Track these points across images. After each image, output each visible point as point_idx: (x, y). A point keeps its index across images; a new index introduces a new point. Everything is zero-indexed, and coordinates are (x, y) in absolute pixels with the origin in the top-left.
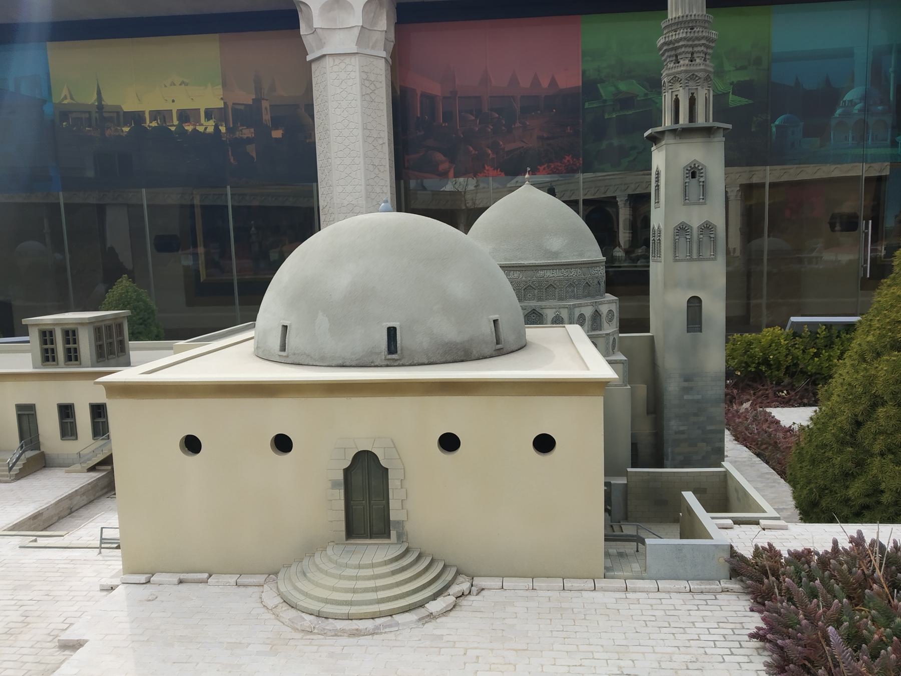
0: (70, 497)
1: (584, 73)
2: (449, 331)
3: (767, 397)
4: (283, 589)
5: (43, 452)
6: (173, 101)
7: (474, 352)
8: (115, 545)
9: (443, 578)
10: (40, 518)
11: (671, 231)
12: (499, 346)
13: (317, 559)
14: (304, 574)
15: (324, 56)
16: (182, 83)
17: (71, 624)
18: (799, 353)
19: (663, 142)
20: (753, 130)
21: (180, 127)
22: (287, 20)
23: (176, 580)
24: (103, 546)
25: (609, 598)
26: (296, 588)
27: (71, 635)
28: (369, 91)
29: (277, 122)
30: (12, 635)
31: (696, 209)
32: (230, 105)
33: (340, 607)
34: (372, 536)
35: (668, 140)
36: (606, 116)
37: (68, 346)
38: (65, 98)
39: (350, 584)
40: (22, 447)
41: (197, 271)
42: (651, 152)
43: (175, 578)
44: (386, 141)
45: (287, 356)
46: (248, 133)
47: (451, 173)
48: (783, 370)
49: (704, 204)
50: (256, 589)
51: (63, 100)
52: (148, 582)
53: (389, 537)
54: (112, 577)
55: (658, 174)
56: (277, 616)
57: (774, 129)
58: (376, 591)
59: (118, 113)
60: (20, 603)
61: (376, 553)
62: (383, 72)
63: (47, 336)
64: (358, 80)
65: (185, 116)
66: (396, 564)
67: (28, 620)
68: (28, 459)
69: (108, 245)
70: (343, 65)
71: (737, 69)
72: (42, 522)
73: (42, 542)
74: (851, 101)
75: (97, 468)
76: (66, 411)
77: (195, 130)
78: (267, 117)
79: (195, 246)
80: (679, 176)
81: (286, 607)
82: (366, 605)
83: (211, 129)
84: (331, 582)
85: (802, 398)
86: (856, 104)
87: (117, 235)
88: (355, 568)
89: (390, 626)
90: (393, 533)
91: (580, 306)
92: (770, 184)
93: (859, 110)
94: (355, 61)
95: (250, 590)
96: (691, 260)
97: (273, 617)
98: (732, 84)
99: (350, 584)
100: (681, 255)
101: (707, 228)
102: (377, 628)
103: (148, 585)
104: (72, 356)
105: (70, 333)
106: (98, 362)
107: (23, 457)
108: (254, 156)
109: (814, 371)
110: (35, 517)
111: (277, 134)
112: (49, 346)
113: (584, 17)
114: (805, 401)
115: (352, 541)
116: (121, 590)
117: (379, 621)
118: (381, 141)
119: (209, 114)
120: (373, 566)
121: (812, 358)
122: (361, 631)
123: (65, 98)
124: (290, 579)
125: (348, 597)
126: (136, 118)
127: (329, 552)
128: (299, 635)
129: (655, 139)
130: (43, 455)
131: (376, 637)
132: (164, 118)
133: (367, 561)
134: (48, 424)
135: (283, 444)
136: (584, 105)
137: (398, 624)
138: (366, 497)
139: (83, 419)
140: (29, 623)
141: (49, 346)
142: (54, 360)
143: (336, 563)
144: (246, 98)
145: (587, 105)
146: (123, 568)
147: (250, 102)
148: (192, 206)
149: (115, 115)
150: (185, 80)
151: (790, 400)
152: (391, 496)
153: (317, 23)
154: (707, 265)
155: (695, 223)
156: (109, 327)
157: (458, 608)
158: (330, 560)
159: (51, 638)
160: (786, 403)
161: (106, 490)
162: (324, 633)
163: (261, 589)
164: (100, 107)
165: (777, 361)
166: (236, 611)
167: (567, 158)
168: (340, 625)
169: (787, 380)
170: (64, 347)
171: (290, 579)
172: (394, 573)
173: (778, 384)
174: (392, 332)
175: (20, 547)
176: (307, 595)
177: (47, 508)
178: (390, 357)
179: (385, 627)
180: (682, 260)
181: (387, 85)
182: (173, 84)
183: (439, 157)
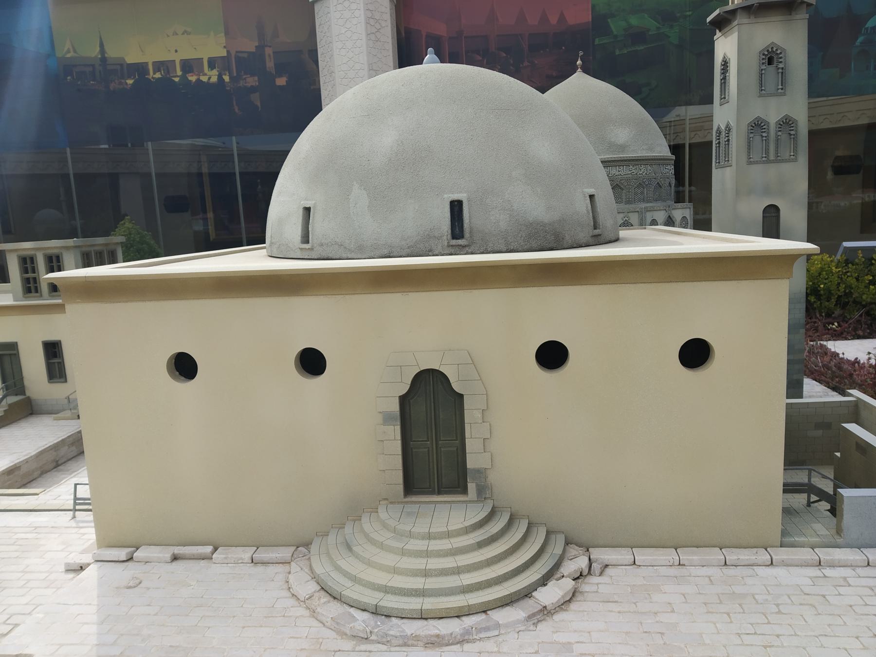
0: (56, 447)
1: (593, 7)
2: (535, 207)
3: (816, 330)
4: (319, 570)
5: (29, 398)
6: (176, 51)
7: (567, 237)
9: (554, 548)
10: (16, 473)
11: (744, 128)
12: (597, 232)
13: (367, 524)
14: (349, 548)
16: (185, 32)
17: (16, 625)
18: (853, 281)
19: (736, 23)
21: (184, 77)
23: (168, 556)
24: (78, 507)
25: (802, 577)
26: (338, 569)
28: (374, 30)
29: (281, 69)
31: (773, 102)
32: (233, 54)
33: (405, 599)
35: (740, 19)
36: (617, 52)
38: (68, 52)
39: (419, 564)
41: (207, 233)
42: (714, 42)
43: (166, 553)
45: (312, 249)
46: (252, 81)
48: (833, 300)
49: (784, 94)
50: (280, 568)
52: (130, 559)
53: (464, 491)
54: (83, 552)
55: (725, 64)
56: (313, 613)
58: (459, 573)
59: (121, 65)
61: (451, 515)
62: (388, 10)
63: (27, 263)
64: (362, 19)
65: (188, 66)
66: (481, 531)
68: (10, 405)
77: (198, 80)
78: (270, 64)
79: (205, 211)
80: (754, 62)
81: (325, 598)
83: (214, 79)
84: (390, 560)
85: (855, 329)
88: (423, 538)
89: (487, 629)
90: (471, 487)
91: (652, 210)
95: (272, 569)
96: (769, 161)
99: (419, 564)
100: (756, 157)
101: (787, 123)
102: (467, 632)
103: (130, 564)
108: (259, 104)
109: (869, 300)
111: (281, 81)
114: (860, 333)
115: (414, 498)
116: (92, 571)
117: (469, 621)
119: (212, 63)
120: (449, 535)
121: (867, 287)
122: (443, 637)
123: (68, 52)
124: (328, 554)
125: (418, 583)
126: (140, 69)
127: (383, 514)
128: (348, 645)
129: (722, 23)
131: (467, 647)
133: (439, 527)
135: (312, 362)
136: (594, 41)
137: (498, 626)
138: (432, 435)
142: (37, 292)
143: (395, 531)
144: (249, 45)
145: (597, 41)
146: (98, 540)
147: (254, 50)
148: (200, 175)
149: (118, 67)
150: (189, 30)
151: (842, 333)
152: (467, 435)
154: (786, 167)
155: (773, 118)
157: (579, 597)
158: (385, 526)
160: (839, 336)
162: (385, 640)
163: (286, 568)
164: (104, 60)
165: (829, 292)
169: (838, 312)
171: (328, 554)
172: (481, 545)
173: (829, 315)
174: (456, 209)
176: (355, 579)
177: (26, 461)
178: (454, 242)
179: (480, 630)
180: (756, 163)
181: (392, 24)
182: (175, 34)
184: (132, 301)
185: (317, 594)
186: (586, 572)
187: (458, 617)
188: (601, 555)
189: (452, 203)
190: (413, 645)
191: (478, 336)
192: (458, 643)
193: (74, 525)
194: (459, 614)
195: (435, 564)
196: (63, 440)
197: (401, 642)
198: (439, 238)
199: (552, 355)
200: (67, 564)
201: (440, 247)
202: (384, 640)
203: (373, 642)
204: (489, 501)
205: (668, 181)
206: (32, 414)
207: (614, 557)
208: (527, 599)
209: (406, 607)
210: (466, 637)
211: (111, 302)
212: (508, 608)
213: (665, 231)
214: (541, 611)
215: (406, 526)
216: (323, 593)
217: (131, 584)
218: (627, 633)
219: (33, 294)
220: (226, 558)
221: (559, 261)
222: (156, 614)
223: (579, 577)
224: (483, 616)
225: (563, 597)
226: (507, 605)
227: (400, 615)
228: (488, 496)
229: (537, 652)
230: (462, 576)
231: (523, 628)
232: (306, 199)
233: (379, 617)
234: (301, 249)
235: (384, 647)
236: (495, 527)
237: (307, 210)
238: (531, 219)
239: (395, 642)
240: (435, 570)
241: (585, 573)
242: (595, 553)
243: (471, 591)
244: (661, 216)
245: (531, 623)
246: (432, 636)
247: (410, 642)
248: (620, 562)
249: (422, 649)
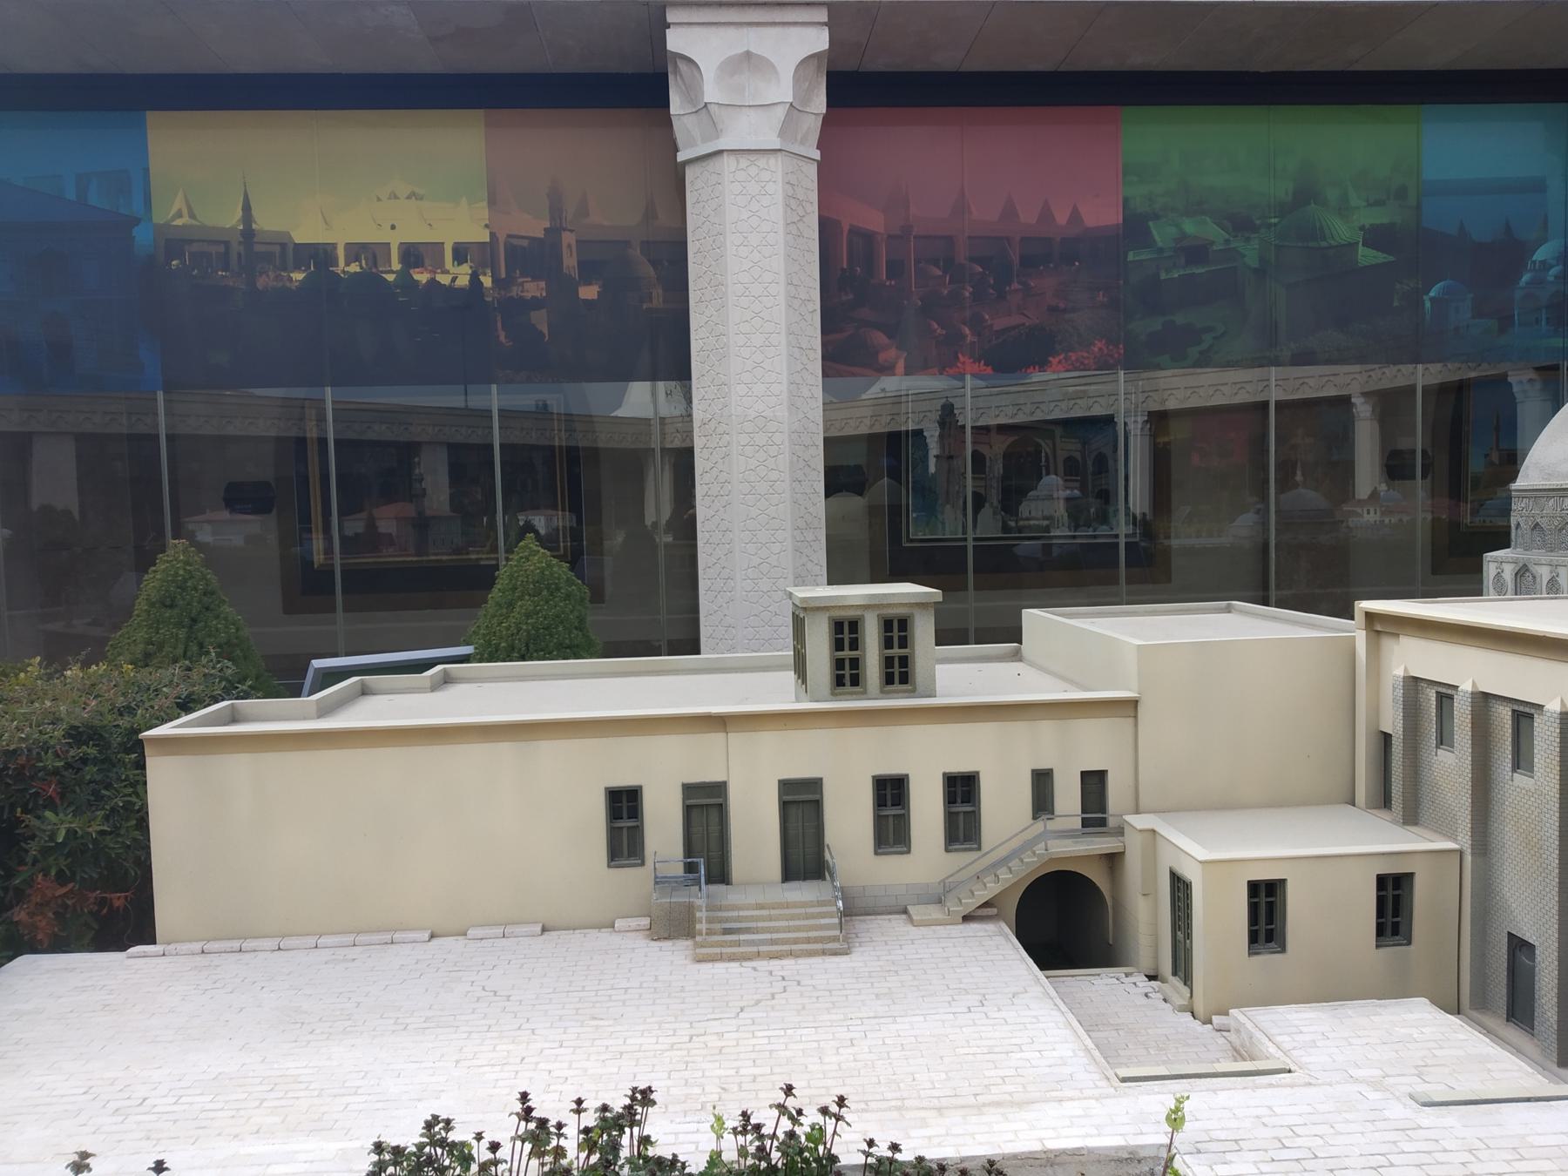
1: (1126, 201)
6: (393, 227)
15: (720, 152)
20: (1396, 304)
21: (404, 275)
22: (638, 88)
29: (589, 270)
32: (502, 239)
36: (1163, 276)
38: (179, 215)
46: (533, 289)
47: (901, 365)
51: (174, 219)
57: (1428, 304)
59: (283, 246)
64: (780, 198)
65: (413, 255)
70: (753, 171)
71: (1369, 205)
74: (1543, 262)
76: (891, 793)
77: (433, 282)
78: (570, 262)
83: (463, 281)
86: (1551, 267)
92: (1278, 403)
93: (1556, 277)
94: (776, 164)
98: (1362, 228)
108: (546, 331)
111: (589, 292)
112: (847, 653)
113: (1128, 112)
119: (460, 253)
123: (179, 215)
126: (320, 256)
132: (375, 257)
134: (848, 821)
139: (927, 808)
144: (534, 226)
145: (1131, 257)
149: (277, 249)
150: (417, 190)
153: (712, 92)
164: (248, 234)
167: (1099, 344)
182: (394, 196)
183: (880, 338)
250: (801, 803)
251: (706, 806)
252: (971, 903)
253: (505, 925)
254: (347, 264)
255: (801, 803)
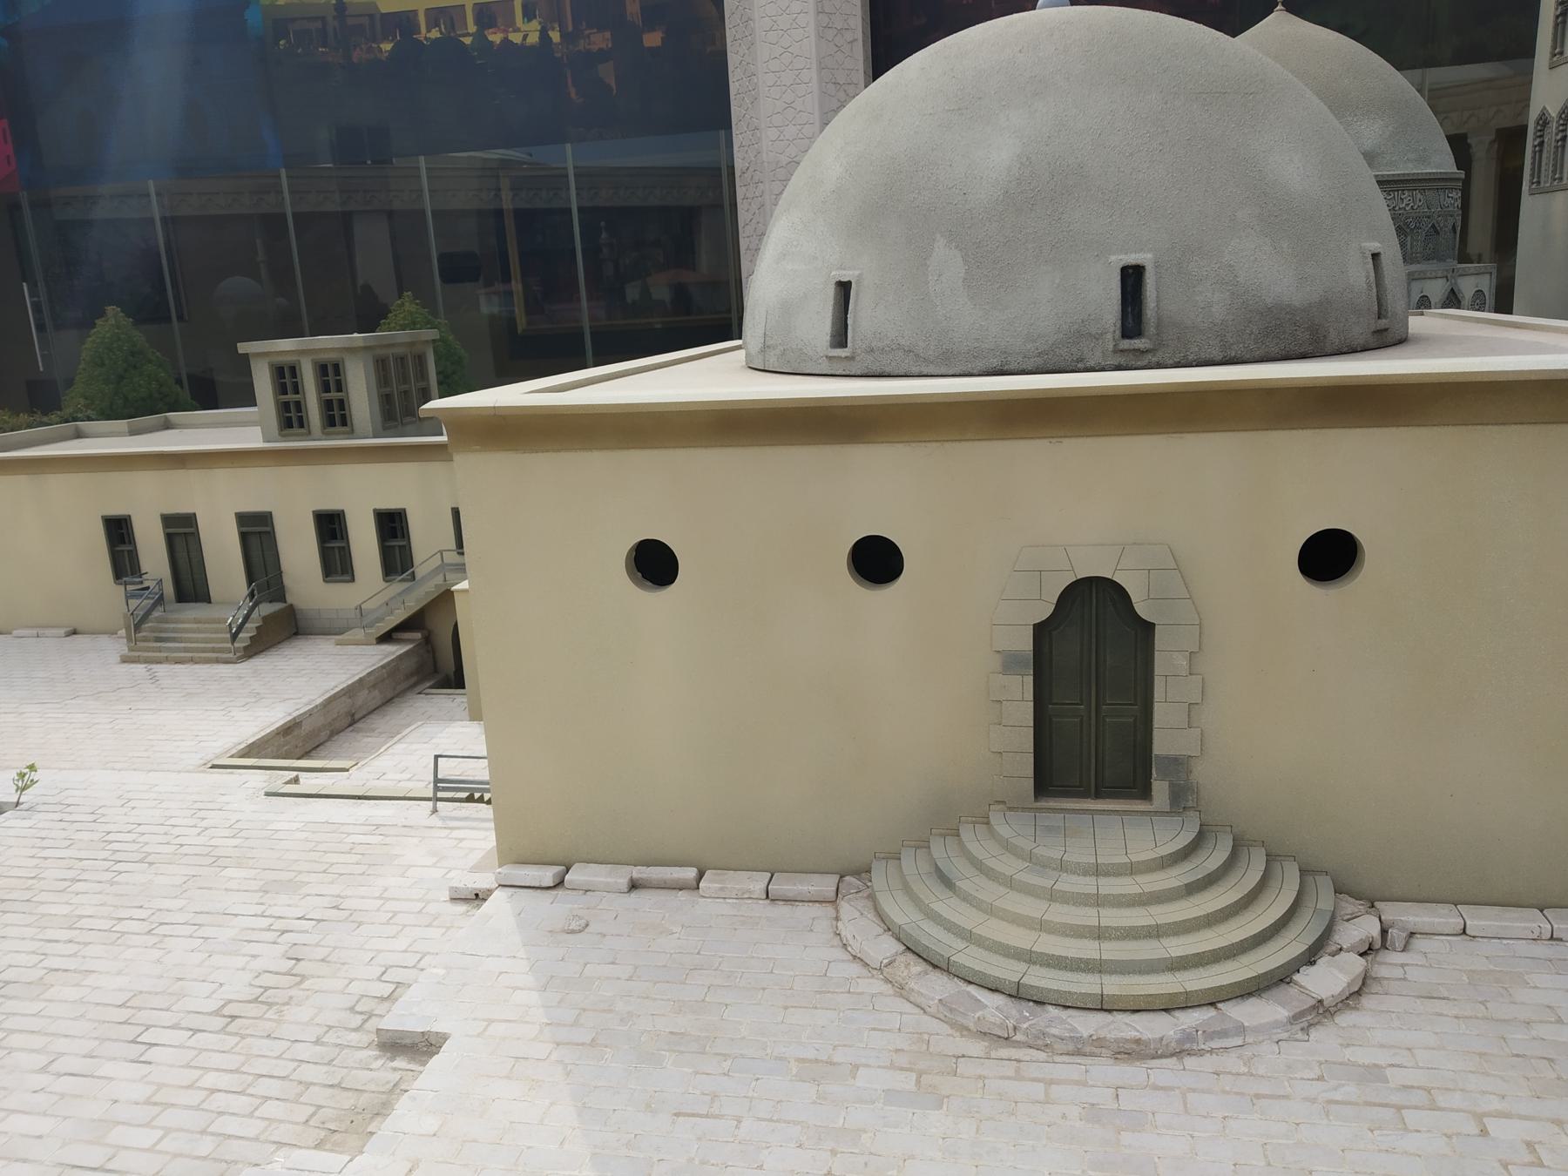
0: (350, 691)
2: (1277, 277)
7: (1333, 335)
8: (465, 795)
9: (1324, 903)
12: (1383, 323)
21: (480, 36)
23: (624, 882)
24: (440, 795)
27: (405, 1018)
30: (270, 1005)
34: (1101, 791)
37: (327, 396)
39: (1088, 916)
40: (252, 595)
41: (512, 322)
43: (621, 877)
44: (859, 35)
45: (851, 358)
46: (600, 40)
50: (816, 910)
52: (559, 884)
53: (1145, 793)
54: (476, 869)
56: (901, 990)
58: (1158, 937)
59: (371, 16)
60: (279, 925)
61: (1127, 838)
63: (285, 377)
66: (1186, 866)
67: (301, 968)
68: (265, 619)
69: (360, 282)
72: (301, 741)
73: (309, 782)
75: (395, 635)
76: (330, 526)
77: (506, 41)
79: (507, 278)
81: (918, 967)
82: (1141, 972)
83: (534, 38)
87: (373, 260)
89: (1223, 1034)
90: (1160, 788)
97: (887, 988)
99: (1088, 916)
102: (1188, 1037)
103: (560, 892)
104: (337, 416)
105: (330, 370)
106: (385, 429)
107: (255, 615)
110: (287, 730)
111: (653, 39)
112: (291, 397)
116: (499, 896)
118: (849, 36)
120: (1132, 869)
122: (1147, 1043)
125: (1088, 949)
126: (403, 23)
128: (976, 1047)
130: (291, 611)
131: (1189, 1062)
134: (299, 551)
137: (1241, 1030)
138: (1092, 694)
139: (364, 541)
140: (304, 978)
141: (291, 397)
142: (344, 423)
143: (1030, 857)
148: (499, 213)
156: (401, 360)
159: (358, 1020)
161: (414, 679)
162: (1041, 1042)
166: (790, 966)
168: (1088, 1025)
170: (320, 398)
172: (1193, 889)
175: (267, 794)
176: (969, 937)
177: (310, 713)
178: (1126, 344)
184: (567, 450)
185: (902, 958)
186: (1378, 945)
187: (1165, 1010)
188: (1406, 915)
189: (1124, 270)
190: (1092, 1055)
191: (1190, 521)
192: (1172, 1055)
193: (440, 824)
194: (1169, 1005)
195: (1113, 917)
196: (361, 680)
197: (1071, 1047)
198: (1097, 337)
199: (1329, 556)
200: (453, 889)
201: (1098, 354)
202: (1040, 1042)
203: (1019, 1045)
204: (1192, 813)
205: (1451, 221)
206: (296, 634)
207: (1426, 919)
208: (1284, 986)
209: (1074, 988)
210: (1187, 1046)
211: (532, 451)
212: (1253, 1000)
213: (1478, 320)
214: (1314, 1007)
215: (1051, 850)
216: (910, 956)
217: (574, 926)
218: (1481, 1055)
219: (296, 430)
220: (722, 889)
221: (1325, 384)
222: (630, 979)
223: (1367, 951)
224: (1209, 1013)
225: (1349, 985)
226: (1250, 994)
227: (1061, 1002)
228: (1190, 804)
229: (1320, 1078)
230: (1165, 942)
231: (1285, 1035)
232: (841, 268)
233: (1024, 1003)
234: (830, 358)
235: (1042, 1055)
236: (1214, 858)
237: (844, 288)
238: (1269, 301)
239: (1059, 1046)
240: (1117, 929)
241: (1378, 945)
242: (1390, 911)
243: (1185, 968)
244: (1436, 289)
245: (1298, 1027)
246: (1127, 1041)
247: (1087, 1049)
248: (1440, 930)
249: (1112, 1061)
250: (257, 532)
251: (181, 532)
252: (385, 627)
253: (40, 628)
254: (429, 31)
255: (257, 532)
